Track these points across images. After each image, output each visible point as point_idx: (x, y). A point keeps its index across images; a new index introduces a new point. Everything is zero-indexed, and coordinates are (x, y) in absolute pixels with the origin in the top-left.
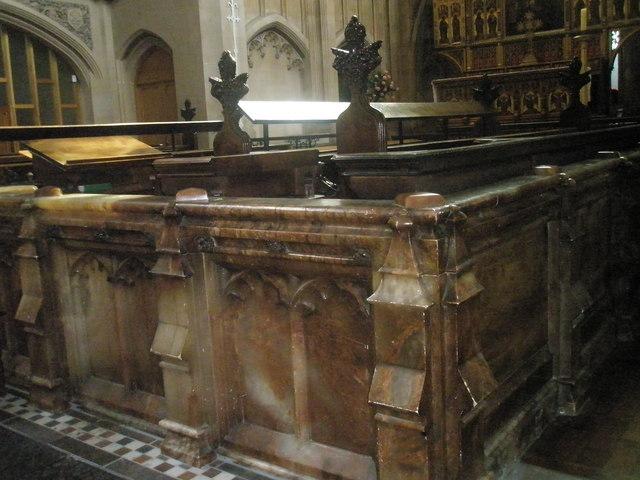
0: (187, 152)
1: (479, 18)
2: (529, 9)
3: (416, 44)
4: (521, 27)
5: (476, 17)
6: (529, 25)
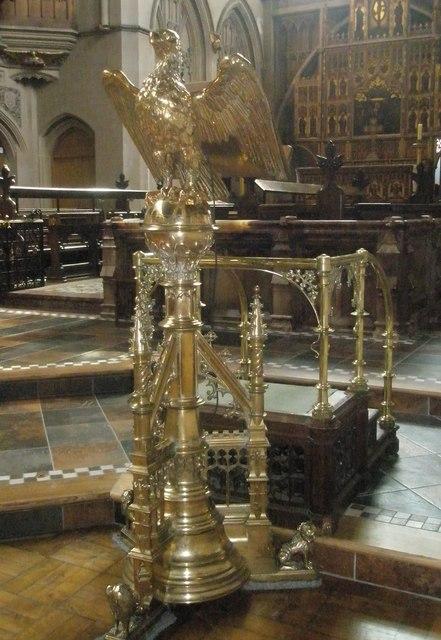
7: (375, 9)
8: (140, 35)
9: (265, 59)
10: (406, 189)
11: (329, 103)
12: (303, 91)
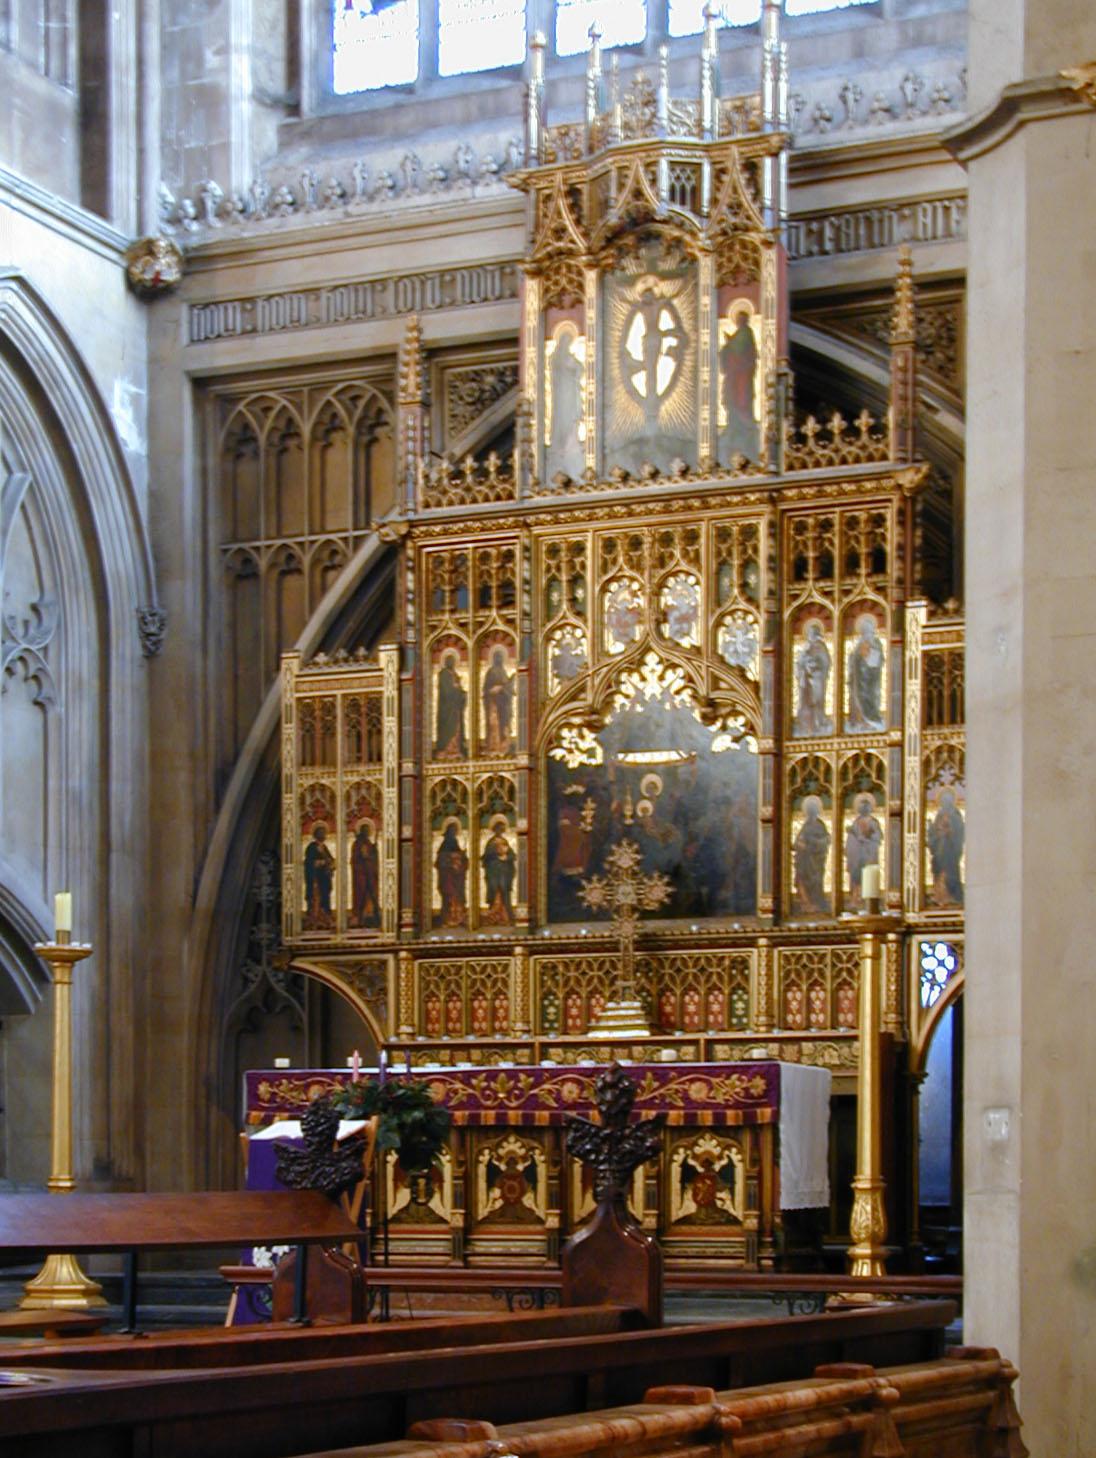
0: (468, 893)
1: (450, 845)
2: (633, 833)
3: (216, 915)
4: (593, 894)
5: (438, 841)
7: (636, 347)
8: (38, 595)
9: (157, 565)
10: (755, 1177)
11: (436, 772)
12: (315, 717)
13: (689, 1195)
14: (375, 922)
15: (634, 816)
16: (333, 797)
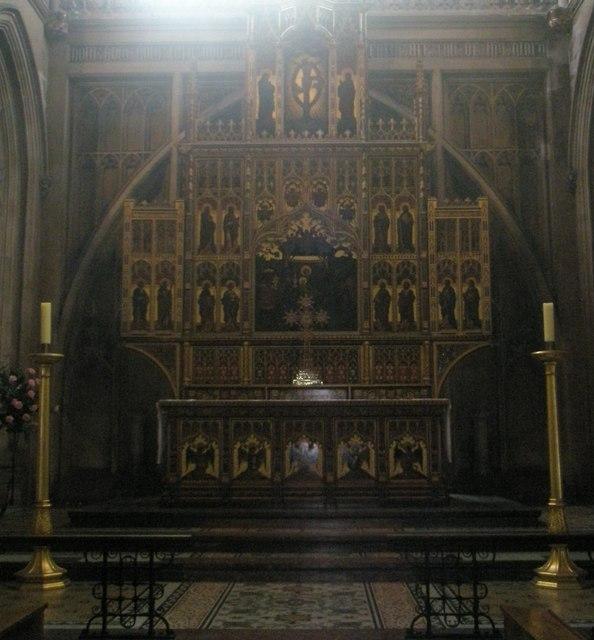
1: (206, 293)
6: (306, 319)
13: (399, 464)
14: (170, 326)
15: (298, 284)
16: (455, 267)
